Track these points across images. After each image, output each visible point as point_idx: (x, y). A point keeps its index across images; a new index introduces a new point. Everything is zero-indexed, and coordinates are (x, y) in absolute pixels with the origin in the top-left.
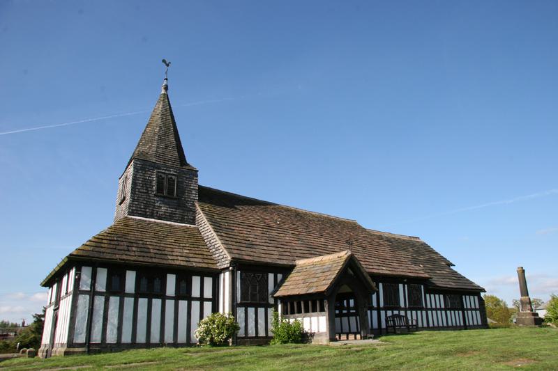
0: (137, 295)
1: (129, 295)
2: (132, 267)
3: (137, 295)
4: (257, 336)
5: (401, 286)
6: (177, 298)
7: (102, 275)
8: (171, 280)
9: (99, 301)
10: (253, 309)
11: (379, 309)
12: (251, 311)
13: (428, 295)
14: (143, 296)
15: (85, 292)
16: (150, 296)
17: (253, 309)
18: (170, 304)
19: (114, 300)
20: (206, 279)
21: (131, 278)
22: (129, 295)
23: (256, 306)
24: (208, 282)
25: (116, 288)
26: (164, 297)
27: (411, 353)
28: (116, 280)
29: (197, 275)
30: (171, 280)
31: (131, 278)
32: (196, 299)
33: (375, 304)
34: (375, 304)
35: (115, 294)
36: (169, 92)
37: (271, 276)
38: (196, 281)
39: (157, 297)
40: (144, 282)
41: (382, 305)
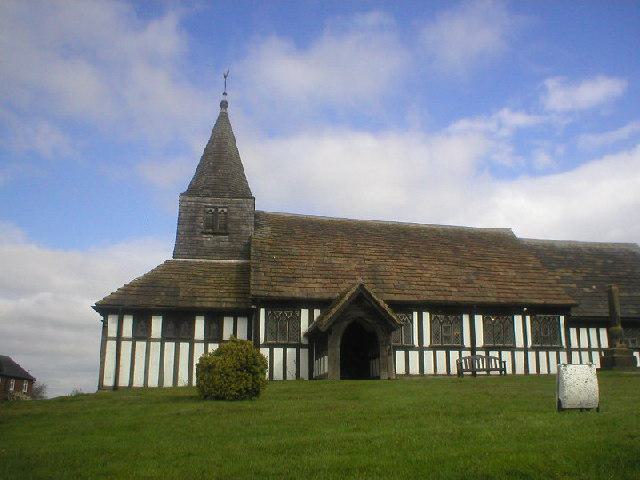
0: (164, 339)
1: (155, 340)
2: (157, 313)
3: (164, 339)
4: (435, 375)
5: (518, 319)
6: (135, 338)
7: (128, 322)
8: (200, 325)
9: (126, 346)
10: (545, 353)
11: (421, 349)
12: (543, 354)
13: (573, 331)
14: (169, 340)
15: (112, 339)
16: (177, 340)
17: (545, 353)
18: (155, 347)
19: (141, 345)
20: (239, 320)
21: (157, 325)
22: (155, 340)
23: (547, 350)
24: (242, 324)
25: (142, 333)
26: (513, 349)
27: (538, 404)
28: (214, 327)
29: (229, 315)
30: (200, 325)
31: (157, 325)
32: (520, 349)
33: (467, 343)
34: (467, 343)
35: (141, 339)
36: (229, 110)
37: (305, 313)
38: (228, 323)
39: (185, 340)
40: (171, 326)
41: (427, 342)
